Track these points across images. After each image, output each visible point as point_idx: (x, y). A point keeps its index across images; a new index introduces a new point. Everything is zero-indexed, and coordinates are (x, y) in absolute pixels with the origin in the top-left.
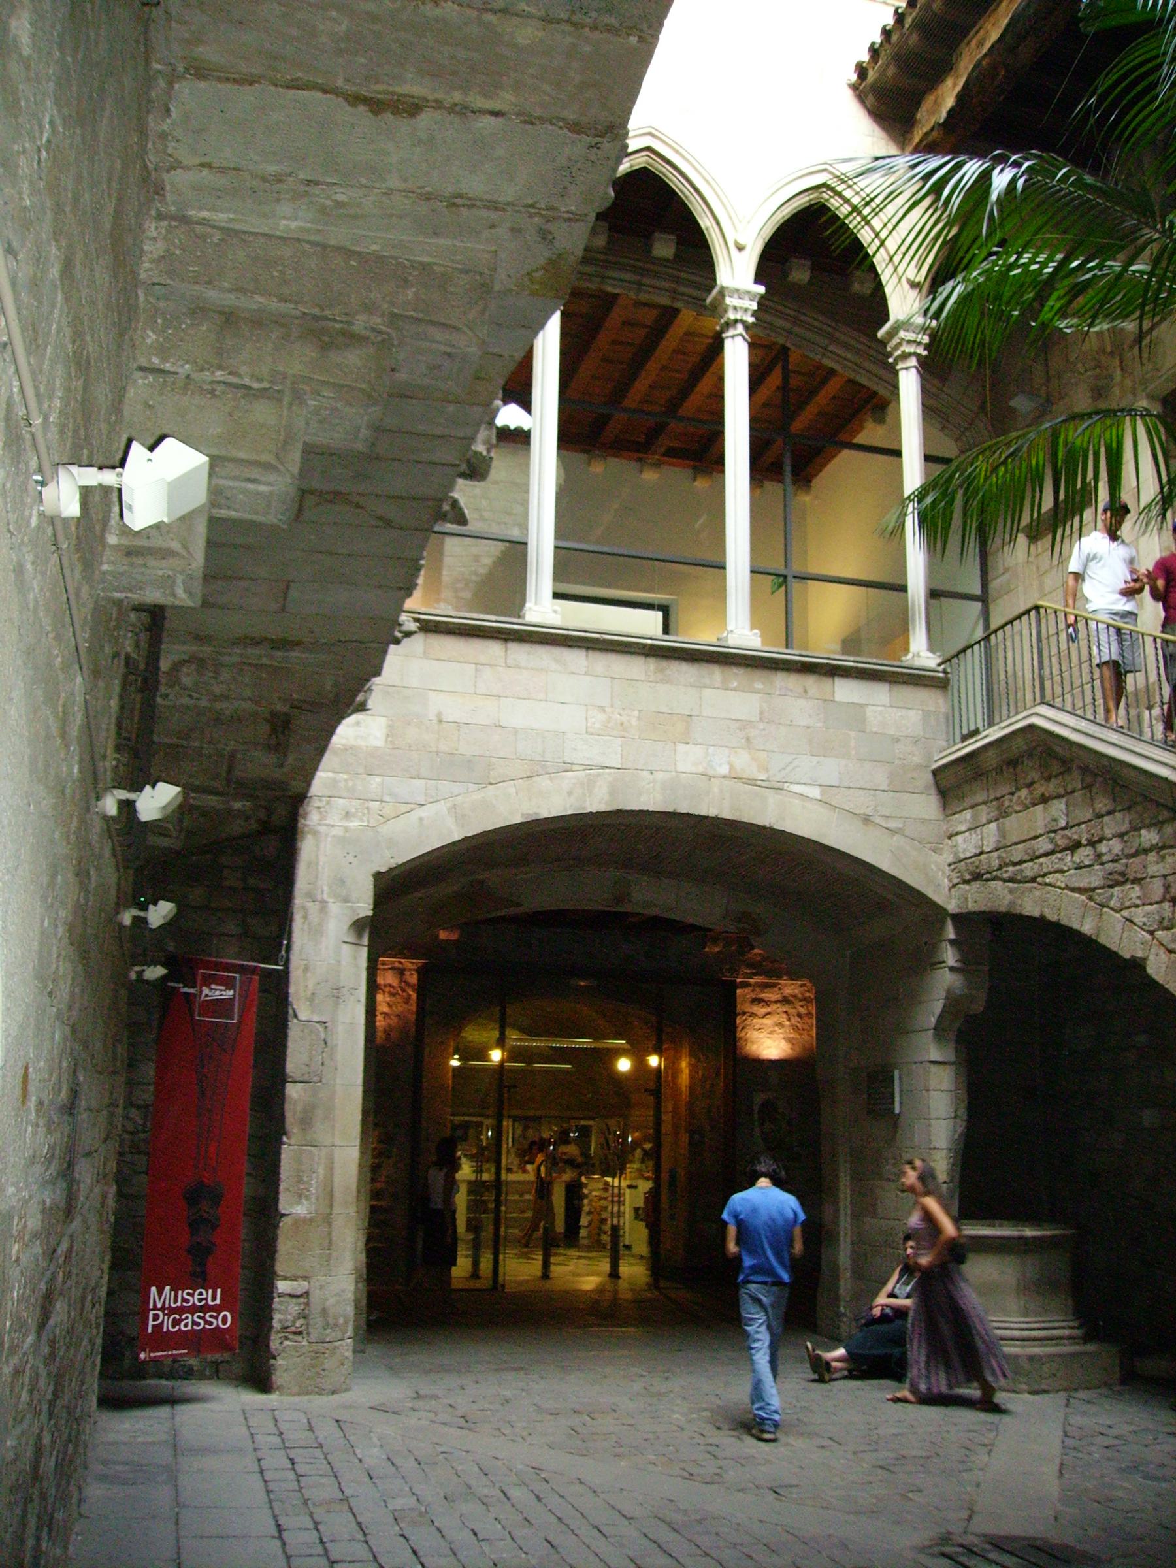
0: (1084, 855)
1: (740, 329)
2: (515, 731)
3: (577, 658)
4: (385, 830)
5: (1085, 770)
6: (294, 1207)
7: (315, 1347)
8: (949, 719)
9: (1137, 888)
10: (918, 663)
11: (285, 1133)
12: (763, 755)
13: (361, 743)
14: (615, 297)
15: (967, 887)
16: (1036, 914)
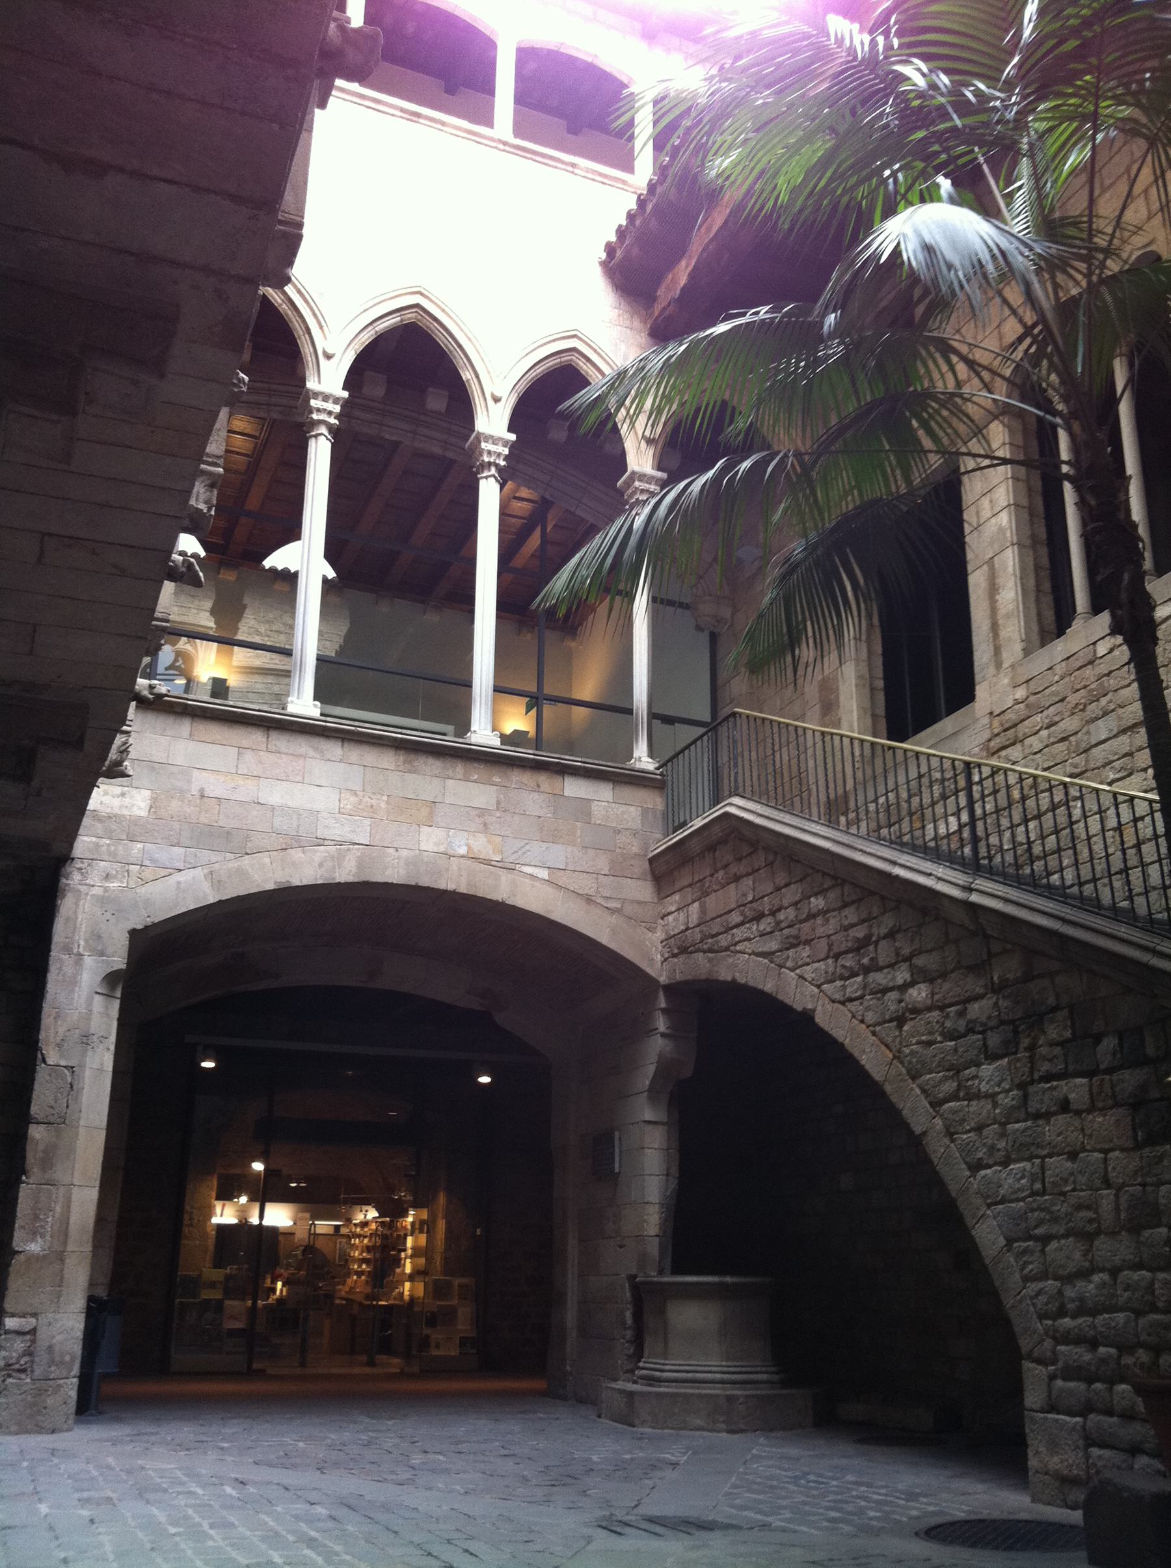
0: (765, 924)
1: (493, 471)
2: (273, 808)
3: (335, 749)
4: (142, 891)
5: (767, 849)
6: (29, 1245)
7: (38, 1384)
8: (665, 815)
9: (807, 948)
10: (638, 766)
11: (24, 1172)
12: (498, 839)
13: (126, 812)
14: (397, 444)
15: (676, 960)
16: (729, 978)
